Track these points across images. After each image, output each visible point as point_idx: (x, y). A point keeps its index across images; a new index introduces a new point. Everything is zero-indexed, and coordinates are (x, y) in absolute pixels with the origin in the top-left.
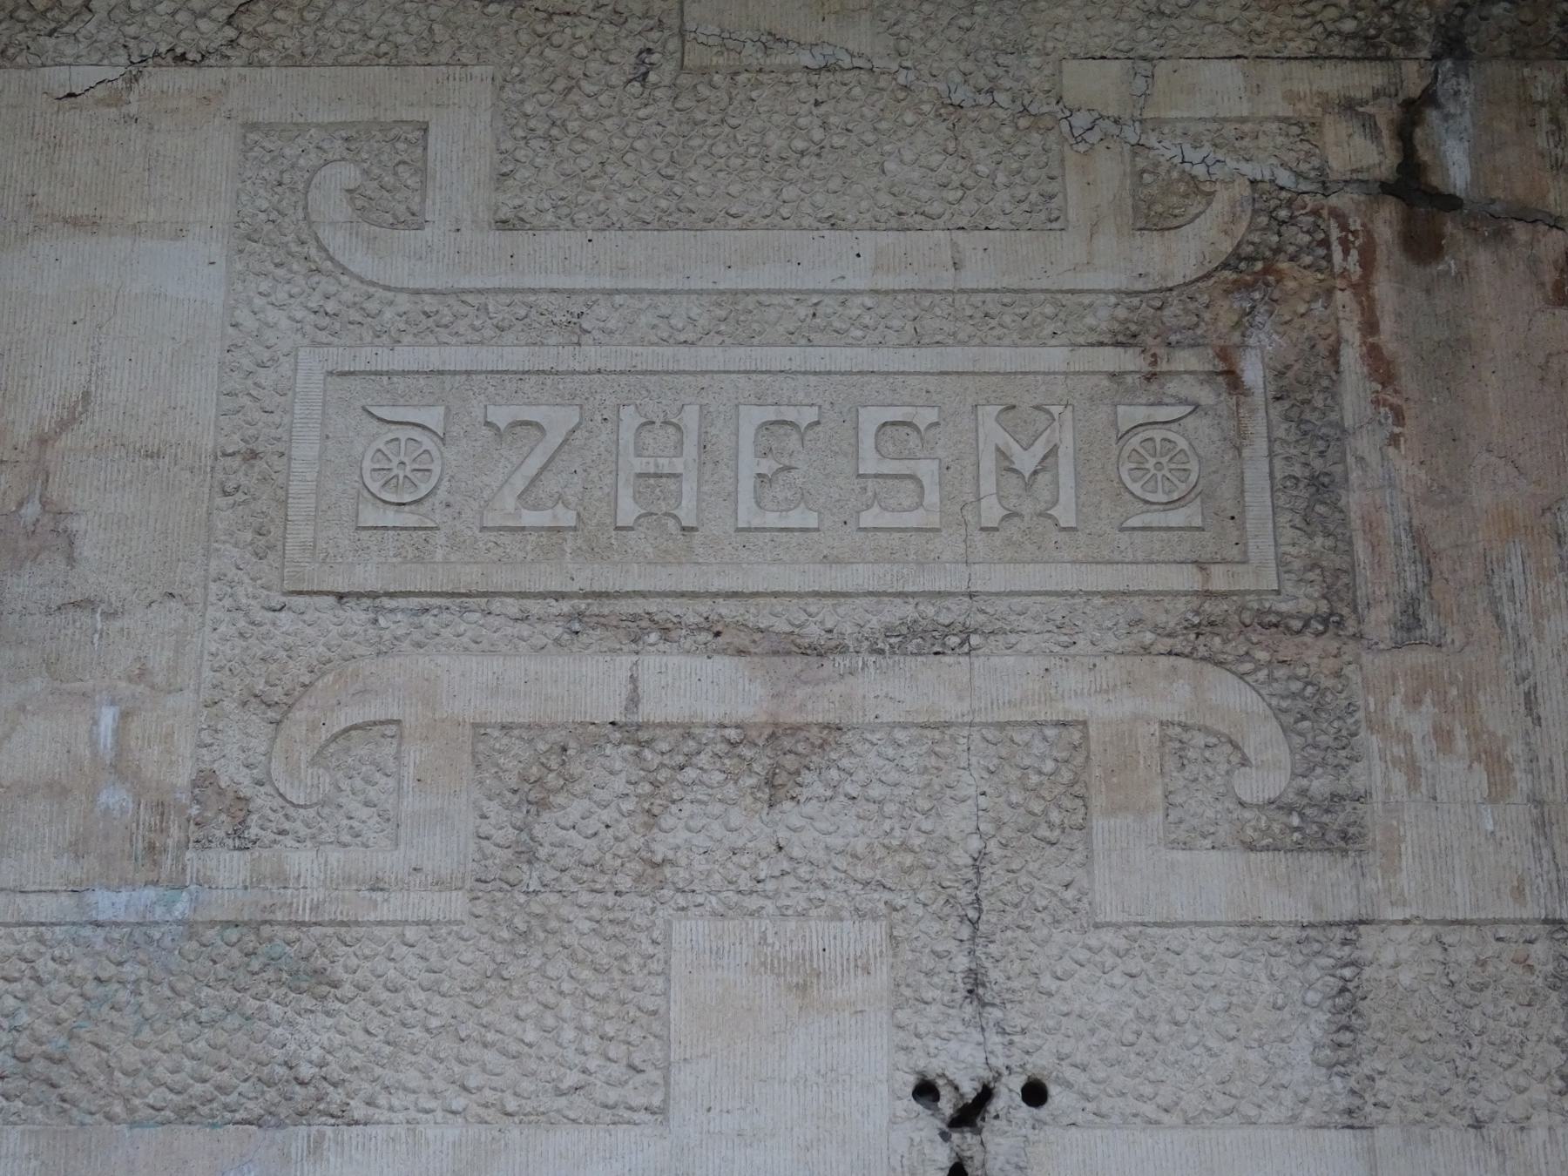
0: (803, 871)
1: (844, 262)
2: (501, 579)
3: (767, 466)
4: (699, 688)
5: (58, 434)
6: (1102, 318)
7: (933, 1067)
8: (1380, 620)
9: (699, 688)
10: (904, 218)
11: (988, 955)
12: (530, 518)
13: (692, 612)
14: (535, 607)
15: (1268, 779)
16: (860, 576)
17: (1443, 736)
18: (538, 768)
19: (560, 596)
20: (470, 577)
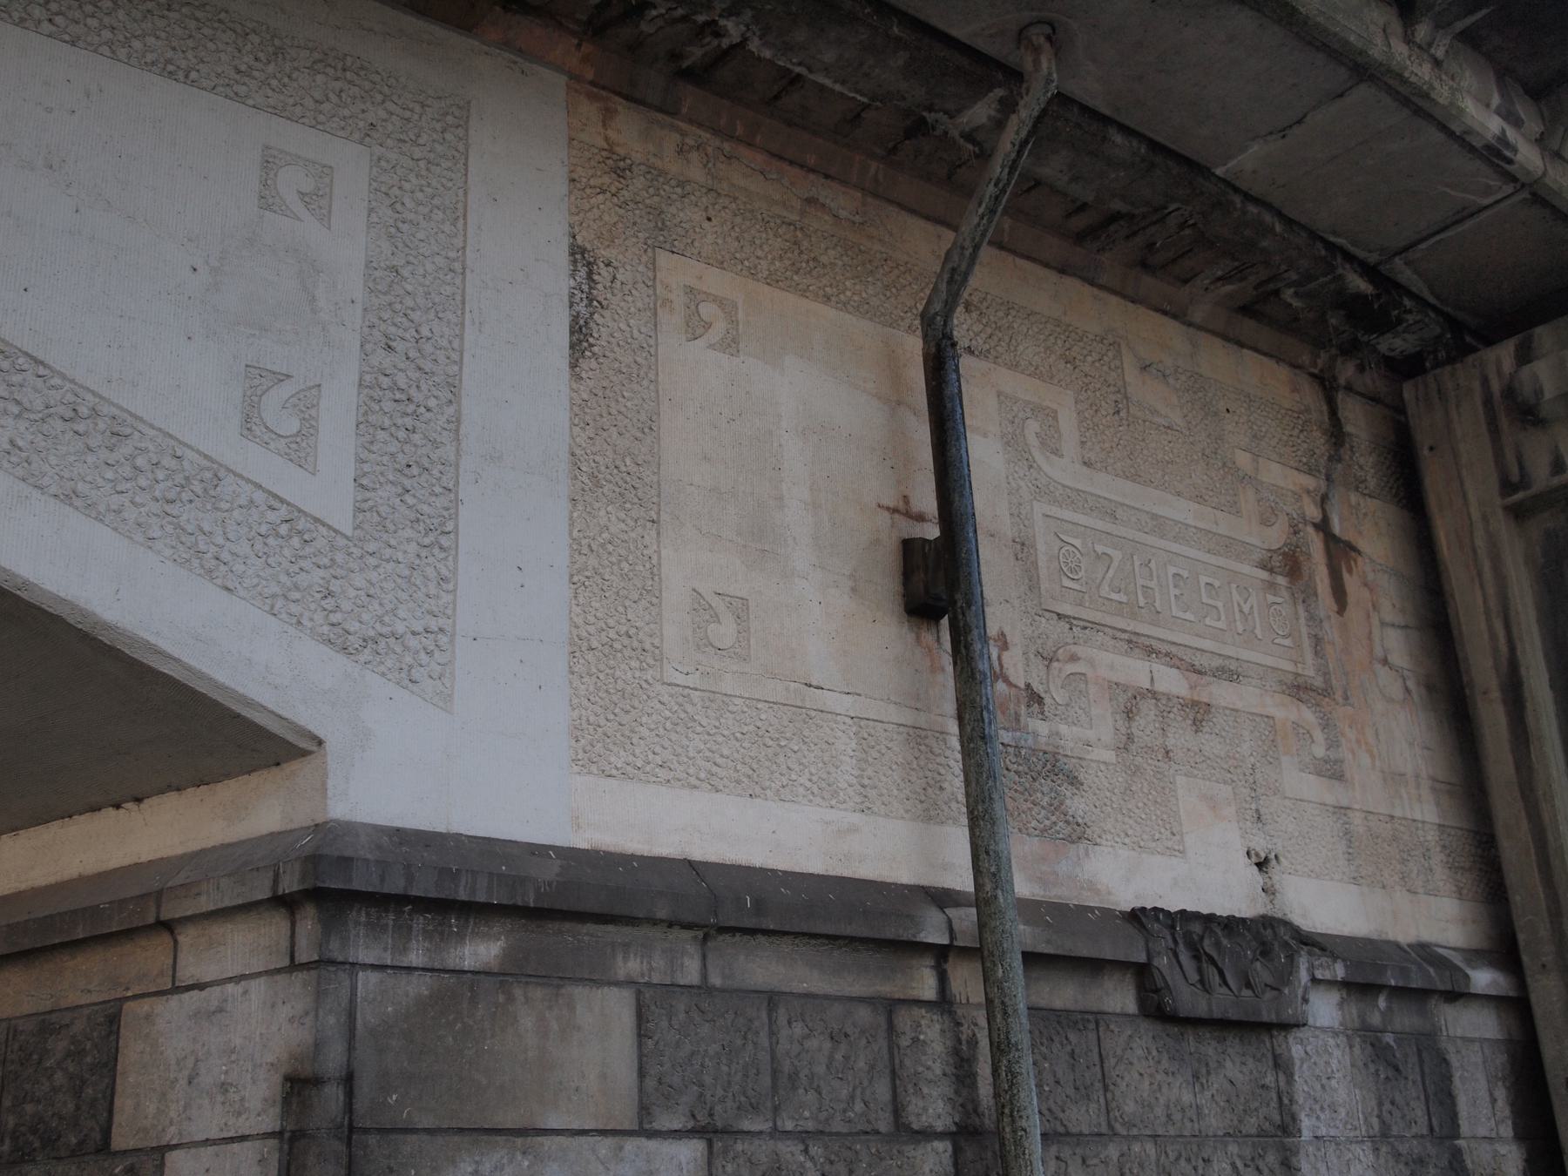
0: (357, 552)
1: (1181, 510)
2: (1109, 620)
3: (1177, 592)
4: (1171, 682)
5: (662, 921)
6: (1256, 556)
7: (1252, 845)
8: (1338, 696)
9: (1171, 682)
10: (1199, 499)
11: (208, 469)
12: (1114, 596)
13: (1164, 648)
14: (1118, 634)
15: (1320, 751)
16: (1207, 644)
17: (1358, 741)
18: (1131, 703)
19: (1124, 631)
20: (1097, 617)
